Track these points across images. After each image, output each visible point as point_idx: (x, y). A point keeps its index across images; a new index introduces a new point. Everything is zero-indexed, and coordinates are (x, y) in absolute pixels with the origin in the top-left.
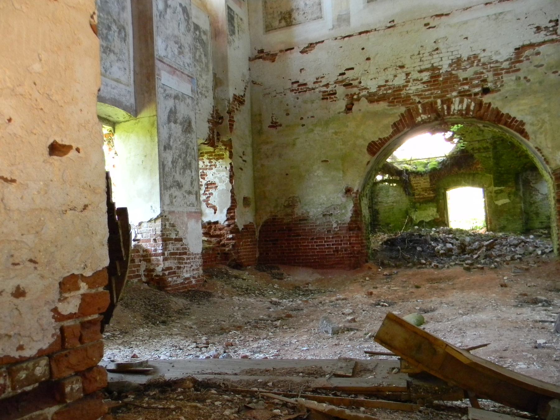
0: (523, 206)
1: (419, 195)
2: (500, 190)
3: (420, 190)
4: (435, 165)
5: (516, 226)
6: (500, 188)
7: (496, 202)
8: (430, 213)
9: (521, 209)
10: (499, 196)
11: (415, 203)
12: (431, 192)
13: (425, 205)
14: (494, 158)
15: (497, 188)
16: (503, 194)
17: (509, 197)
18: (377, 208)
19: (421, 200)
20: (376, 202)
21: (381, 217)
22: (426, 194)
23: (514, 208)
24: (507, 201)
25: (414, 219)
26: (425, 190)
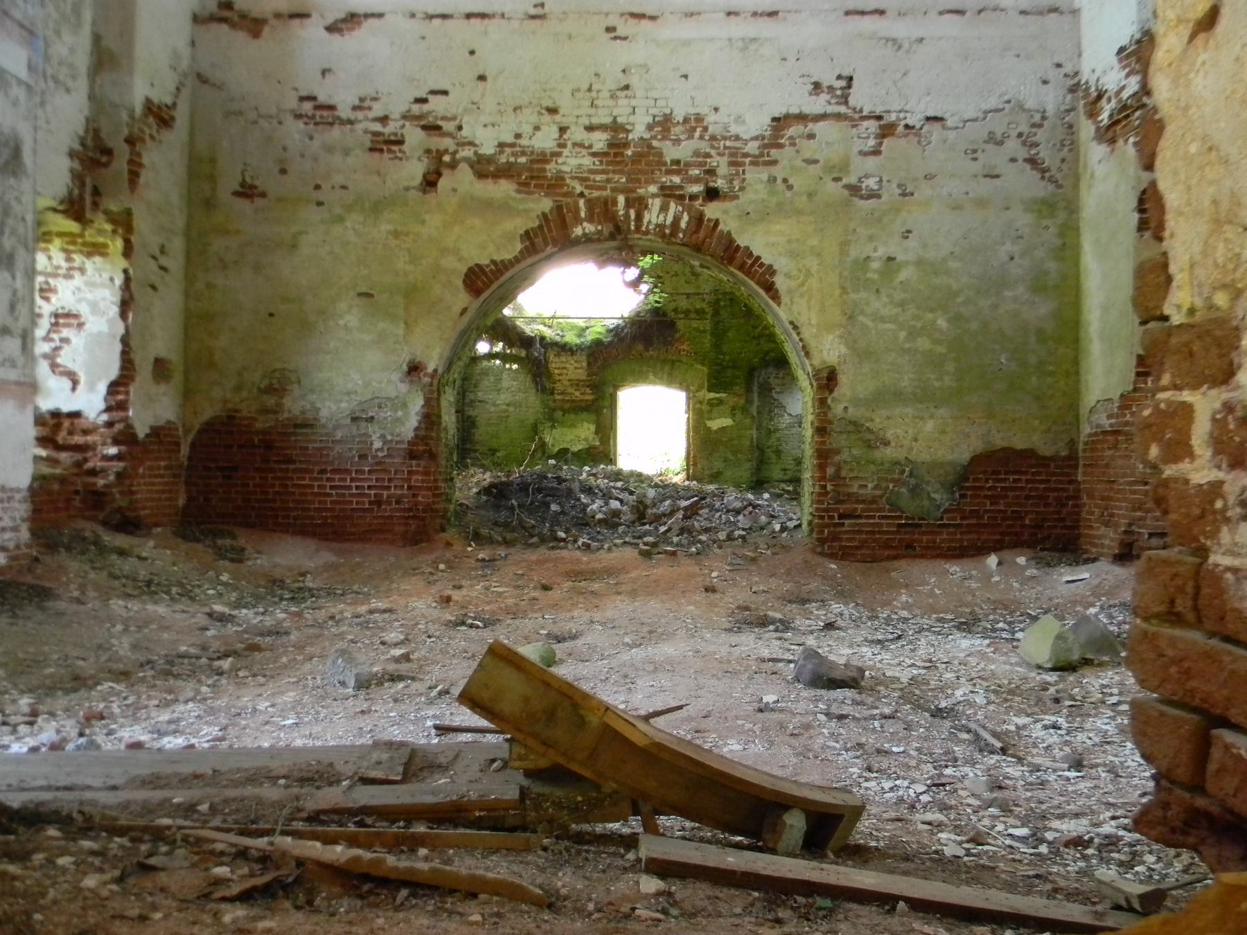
1: (562, 393)
5: (740, 474)
7: (709, 424)
8: (581, 434)
10: (716, 410)
12: (588, 391)
14: (712, 334)
15: (712, 395)
19: (567, 406)
20: (472, 401)
22: (577, 393)
23: (739, 437)
24: (726, 422)
26: (577, 384)
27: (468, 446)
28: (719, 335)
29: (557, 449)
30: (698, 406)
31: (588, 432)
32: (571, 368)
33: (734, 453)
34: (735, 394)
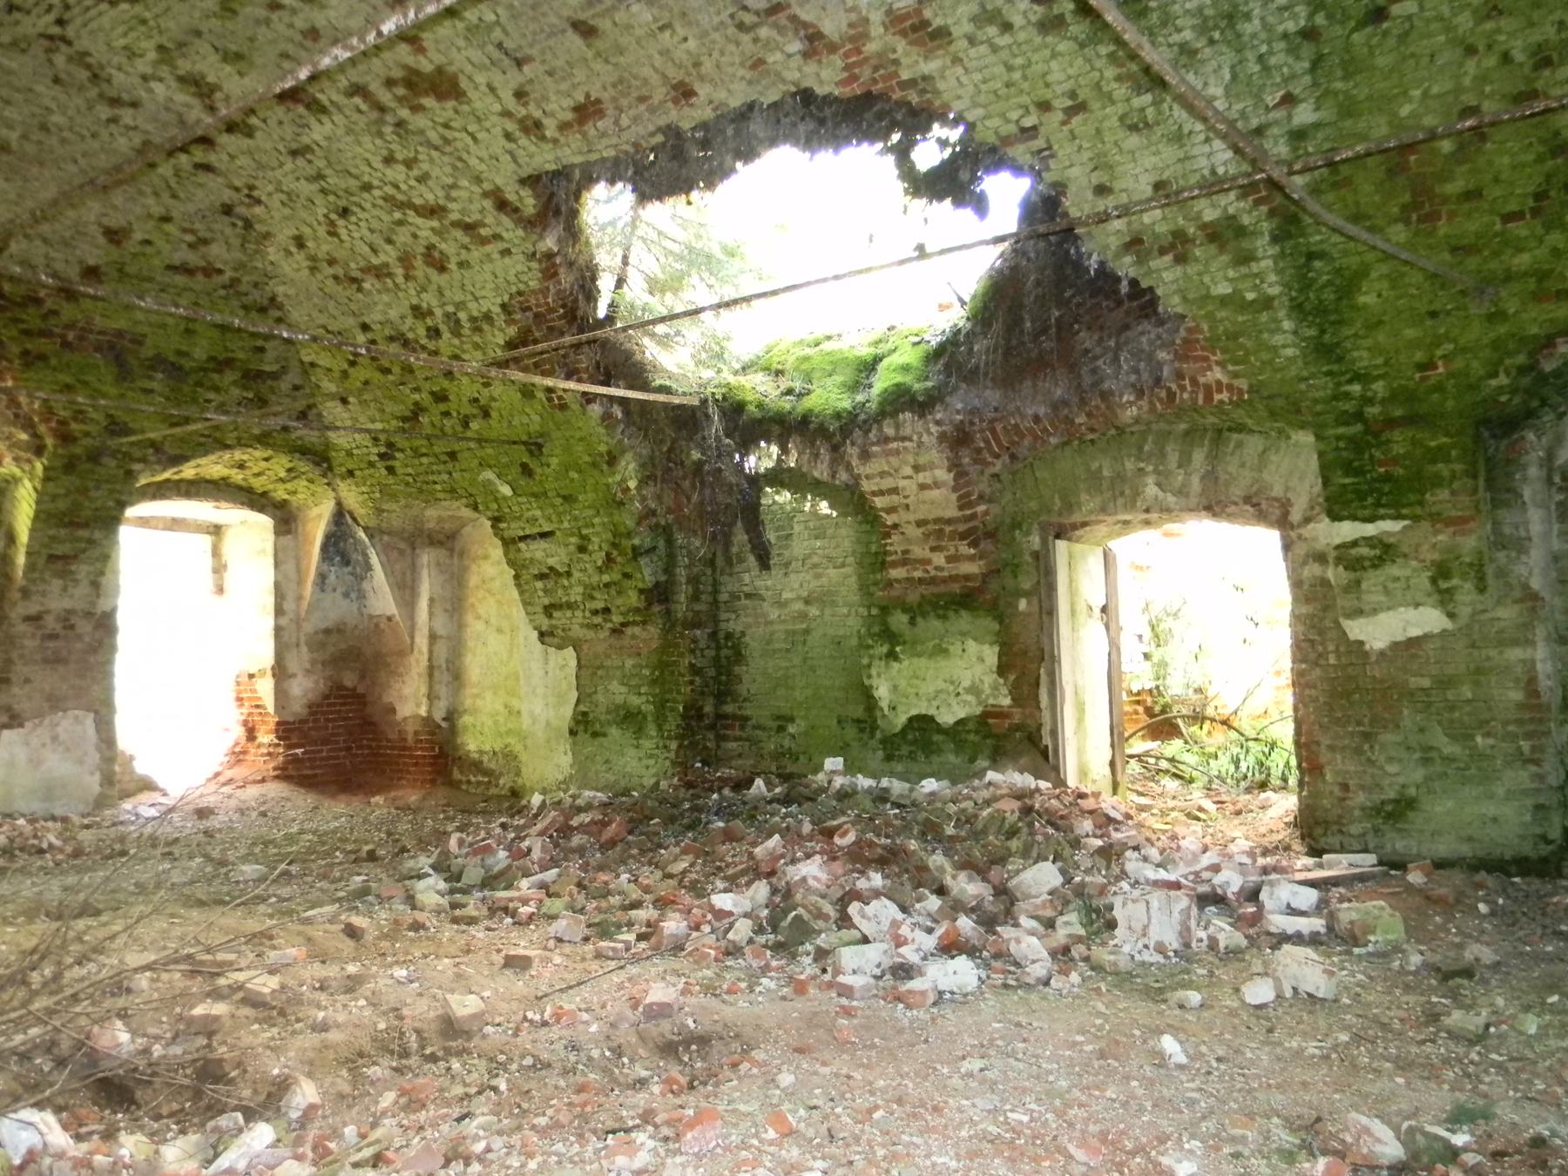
0: (1544, 668)
1: (904, 562)
2: (1369, 541)
3: (914, 532)
4: (906, 368)
5: (1490, 809)
6: (1370, 529)
7: (1356, 629)
8: (952, 677)
9: (1531, 685)
10: (1372, 580)
11: (885, 610)
12: (965, 549)
13: (936, 624)
14: (1297, 309)
15: (1348, 530)
16: (1394, 570)
17: (1445, 599)
18: (734, 626)
19: (913, 597)
20: (735, 597)
21: (754, 676)
22: (939, 559)
23: (1479, 673)
24: (1428, 620)
25: (884, 704)
26: (936, 531)
27: (729, 708)
28: (1323, 306)
29: (901, 720)
30: (1312, 570)
31: (979, 669)
32: (909, 486)
33: (1462, 735)
34: (1435, 518)
